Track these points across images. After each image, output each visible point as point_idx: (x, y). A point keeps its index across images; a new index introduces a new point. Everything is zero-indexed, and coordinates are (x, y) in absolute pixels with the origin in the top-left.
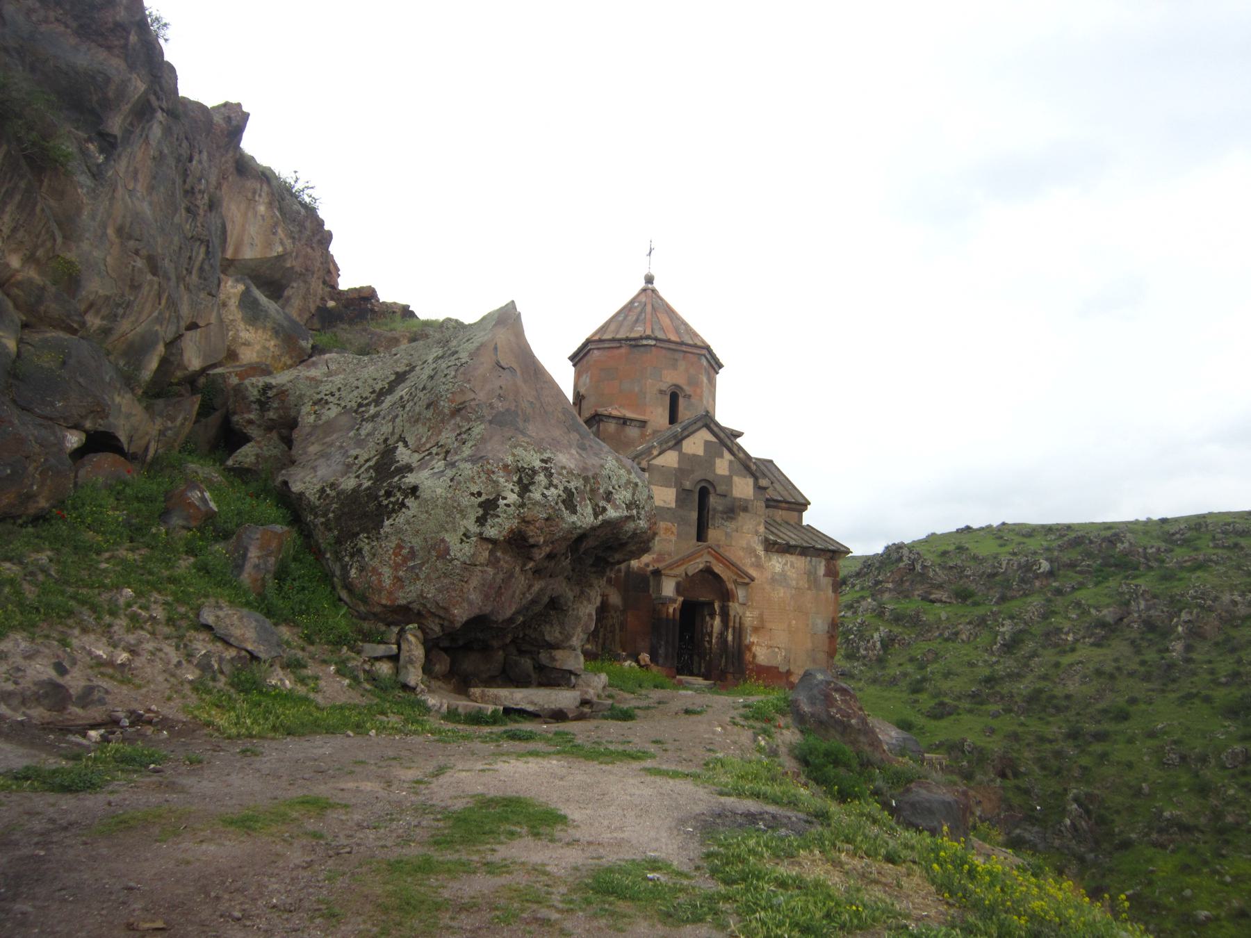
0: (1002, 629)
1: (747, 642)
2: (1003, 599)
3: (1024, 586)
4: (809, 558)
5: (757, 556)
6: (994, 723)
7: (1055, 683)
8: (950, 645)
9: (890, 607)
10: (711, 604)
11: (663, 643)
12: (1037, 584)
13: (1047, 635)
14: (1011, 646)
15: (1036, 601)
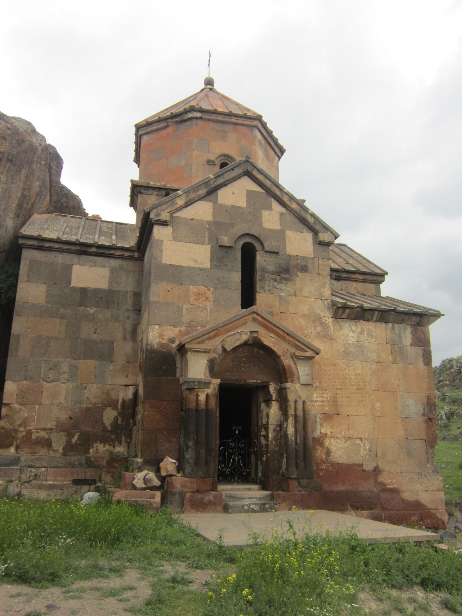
4: (390, 325)
5: (323, 324)
9: (449, 395)
10: (265, 387)
11: (191, 443)
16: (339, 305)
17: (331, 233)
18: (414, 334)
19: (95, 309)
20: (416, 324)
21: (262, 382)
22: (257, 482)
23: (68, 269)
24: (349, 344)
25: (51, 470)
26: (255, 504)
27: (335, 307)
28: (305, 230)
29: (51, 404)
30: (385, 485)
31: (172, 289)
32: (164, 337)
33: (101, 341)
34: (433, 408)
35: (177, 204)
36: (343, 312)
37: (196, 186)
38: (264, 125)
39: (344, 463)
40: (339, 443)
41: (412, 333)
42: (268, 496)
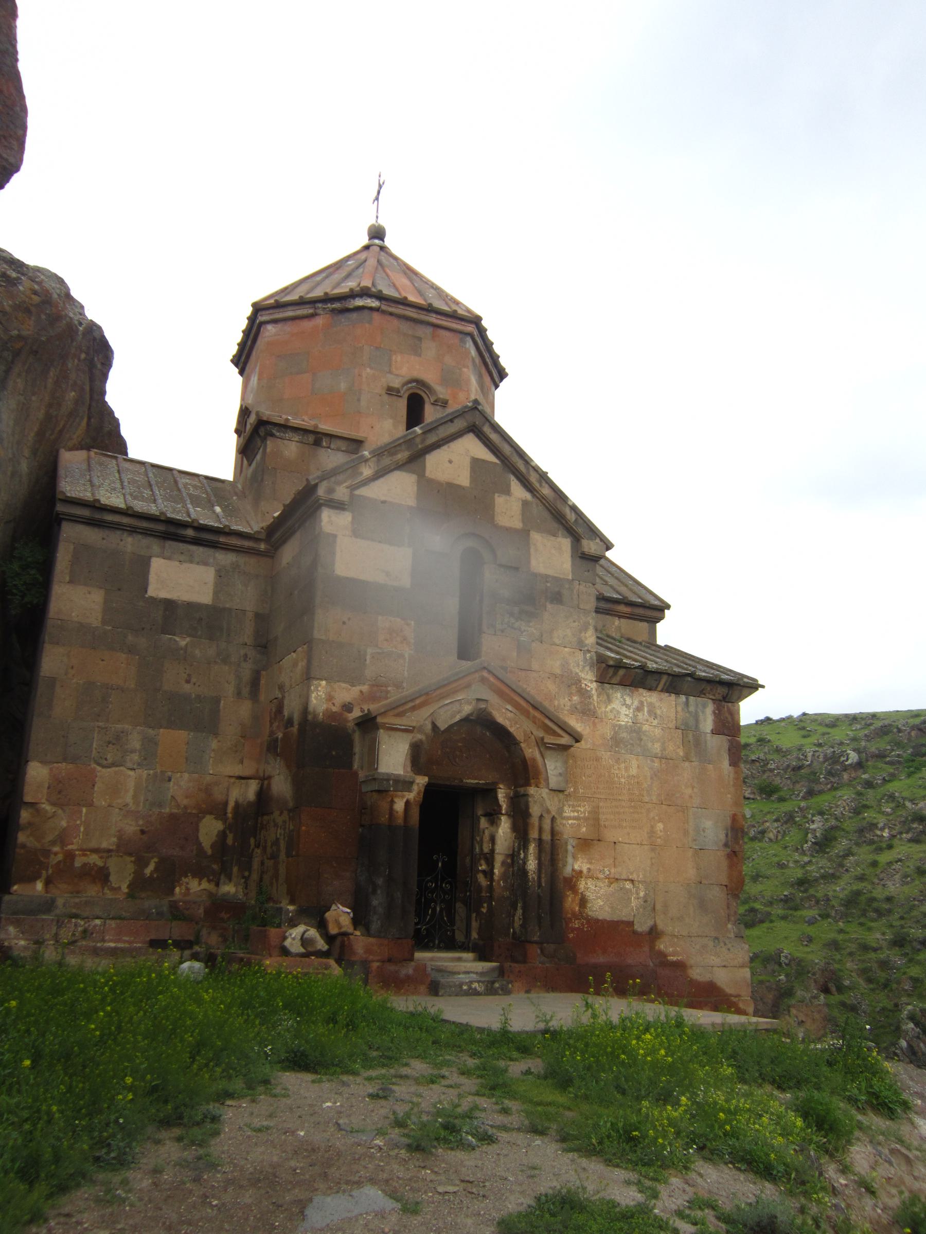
0: (813, 826)
1: (568, 871)
2: (810, 793)
3: (832, 779)
4: (683, 698)
5: (584, 693)
6: (811, 930)
7: (873, 883)
8: (757, 845)
10: (489, 792)
11: (380, 881)
12: (846, 776)
13: (861, 831)
14: (823, 844)
15: (846, 795)
16: (611, 663)
17: (601, 540)
18: (718, 714)
19: (188, 639)
20: (721, 698)
21: (486, 784)
22: (469, 947)
23: (143, 565)
24: (620, 726)
25: (113, 924)
26: (479, 982)
27: (604, 665)
28: (560, 532)
29: (109, 806)
30: (665, 956)
31: (349, 619)
32: (335, 701)
33: (198, 697)
34: (740, 835)
35: (361, 473)
36: (615, 674)
37: (393, 445)
38: (482, 331)
39: (605, 920)
40: (601, 888)
41: (714, 712)
42: (493, 970)
